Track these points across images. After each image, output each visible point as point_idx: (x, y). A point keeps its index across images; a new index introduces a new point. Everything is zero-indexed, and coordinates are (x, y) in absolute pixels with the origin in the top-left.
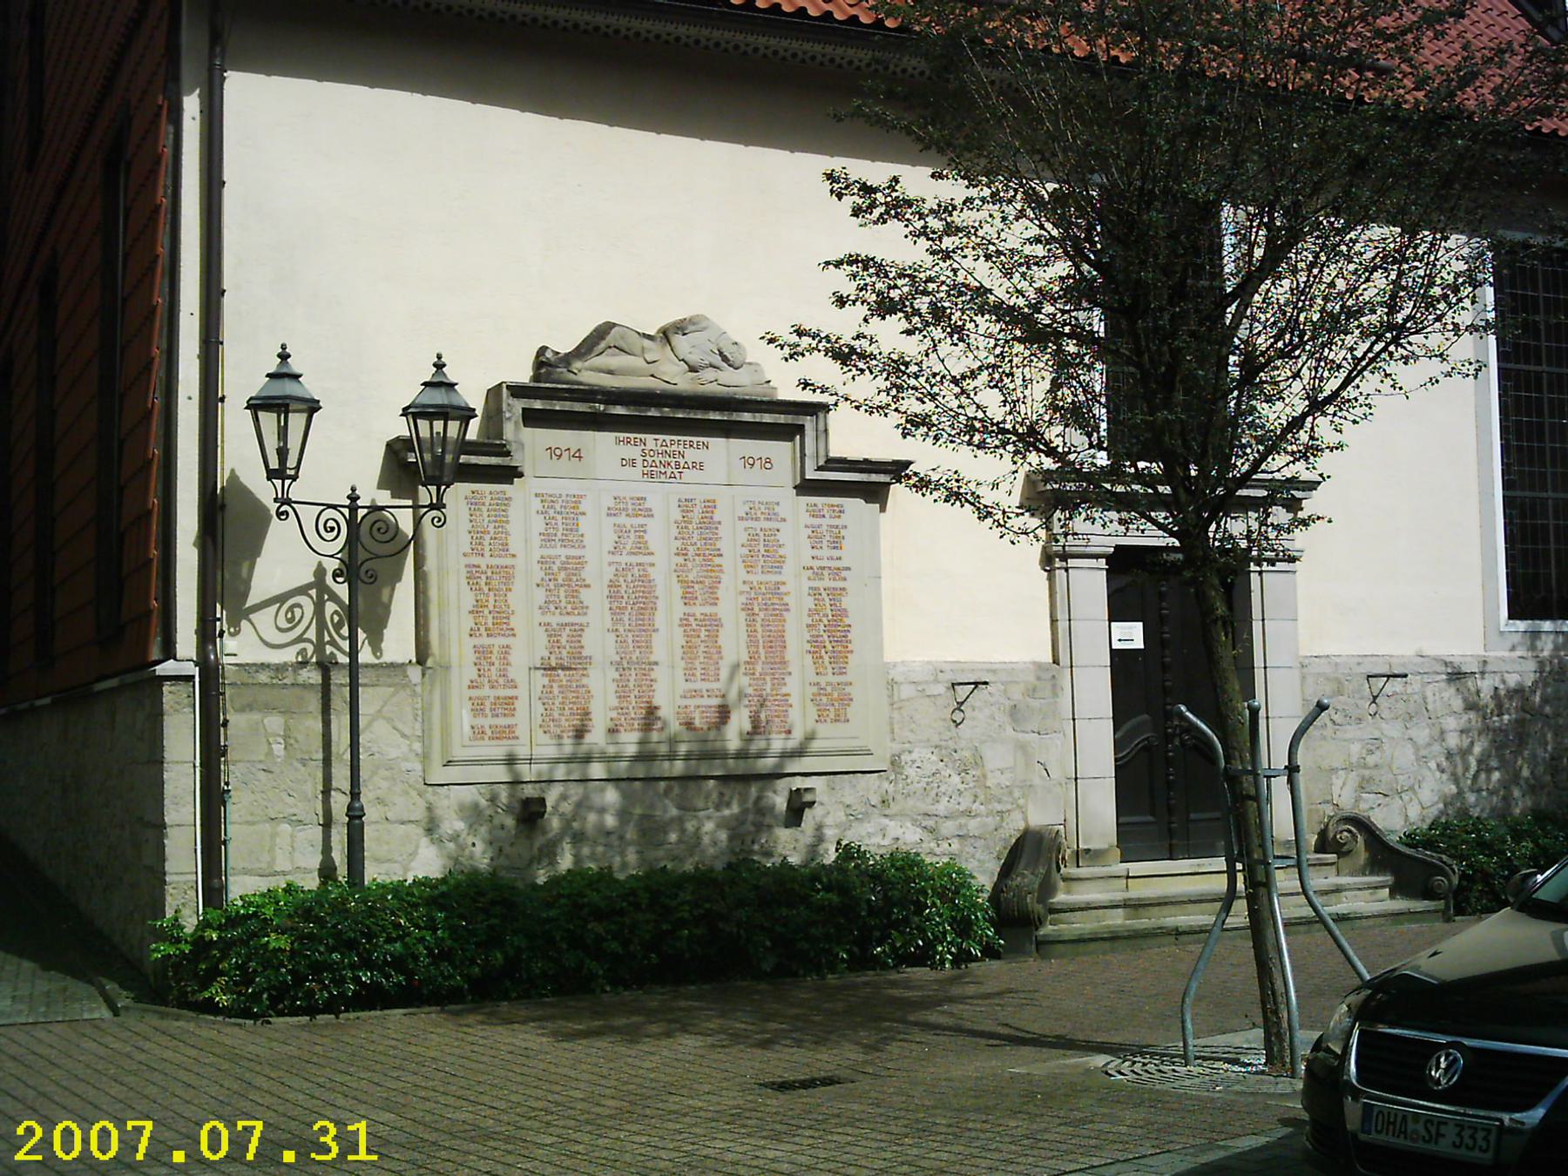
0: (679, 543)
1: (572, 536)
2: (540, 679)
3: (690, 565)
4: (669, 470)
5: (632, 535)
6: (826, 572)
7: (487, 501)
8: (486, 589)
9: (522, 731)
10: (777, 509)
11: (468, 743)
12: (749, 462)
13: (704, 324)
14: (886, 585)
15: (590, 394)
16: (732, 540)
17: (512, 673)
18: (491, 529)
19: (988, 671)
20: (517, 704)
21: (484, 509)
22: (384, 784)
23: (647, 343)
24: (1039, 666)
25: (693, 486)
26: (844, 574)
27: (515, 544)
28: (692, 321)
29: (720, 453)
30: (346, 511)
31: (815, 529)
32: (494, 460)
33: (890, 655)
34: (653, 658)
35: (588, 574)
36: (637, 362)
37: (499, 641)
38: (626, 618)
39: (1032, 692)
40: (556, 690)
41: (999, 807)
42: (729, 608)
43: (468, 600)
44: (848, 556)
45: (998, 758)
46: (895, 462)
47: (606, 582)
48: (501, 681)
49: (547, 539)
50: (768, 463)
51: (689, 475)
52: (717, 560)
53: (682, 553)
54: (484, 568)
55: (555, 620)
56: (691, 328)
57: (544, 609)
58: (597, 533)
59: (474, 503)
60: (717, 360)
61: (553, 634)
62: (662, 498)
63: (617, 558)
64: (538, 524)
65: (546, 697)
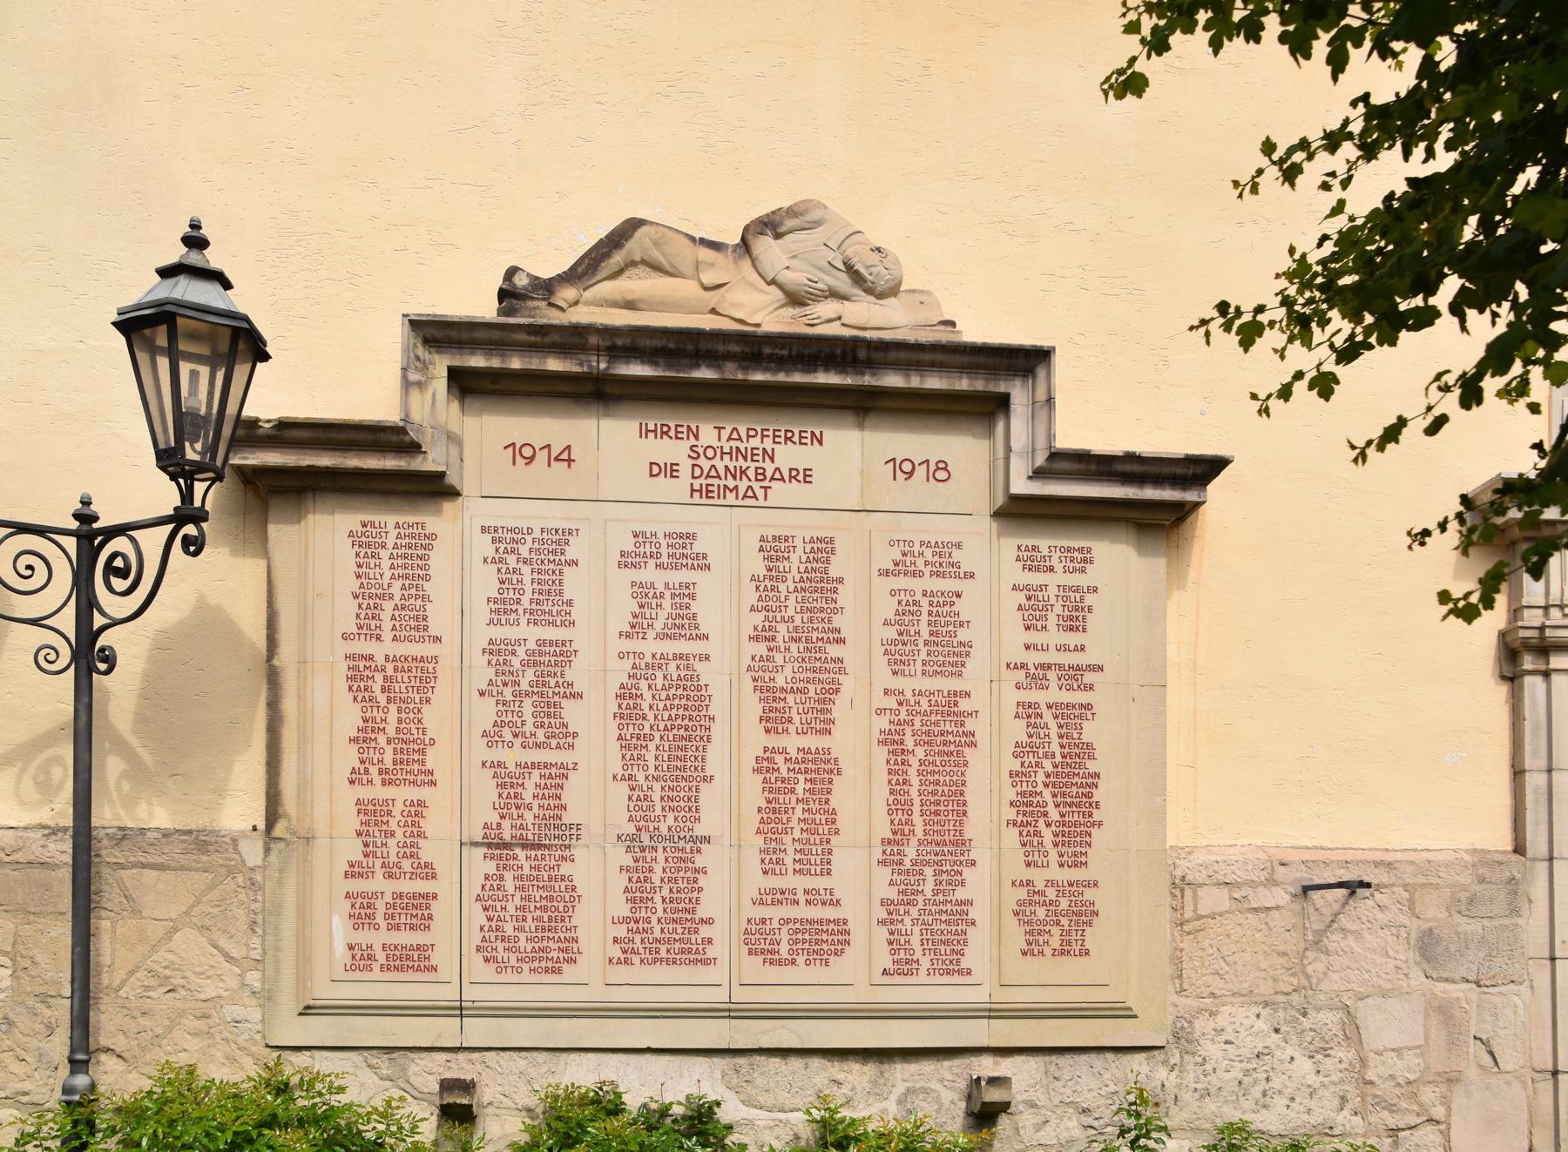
0: (758, 619)
1: (551, 604)
2: (480, 865)
3: (779, 658)
4: (743, 485)
5: (667, 603)
6: (1052, 675)
7: (390, 542)
8: (382, 699)
9: (444, 958)
10: (957, 555)
11: (342, 975)
12: (902, 469)
13: (815, 215)
14: (1178, 701)
15: (574, 339)
16: (864, 612)
17: (427, 852)
18: (396, 589)
19: (1377, 864)
20: (436, 908)
21: (384, 554)
22: (193, 1044)
23: (705, 254)
24: (1483, 858)
25: (790, 513)
26: (1089, 678)
27: (440, 618)
28: (792, 212)
29: (844, 460)
30: (70, 544)
31: (1031, 592)
32: (390, 463)
33: (1178, 832)
34: (700, 830)
35: (577, 674)
36: (685, 288)
37: (402, 794)
38: (650, 756)
39: (1468, 905)
40: (509, 885)
41: (1392, 1121)
42: (854, 737)
43: (350, 717)
44: (1099, 642)
45: (1393, 1027)
46: (1191, 460)
47: (614, 689)
48: (407, 865)
49: (502, 609)
50: (940, 471)
51: (781, 492)
52: (834, 651)
53: (763, 635)
54: (380, 660)
55: (513, 756)
56: (790, 223)
57: (492, 738)
58: (599, 599)
59: (365, 544)
60: (842, 282)
61: (508, 783)
62: (729, 537)
63: (635, 645)
64: (485, 582)
65: (491, 897)
